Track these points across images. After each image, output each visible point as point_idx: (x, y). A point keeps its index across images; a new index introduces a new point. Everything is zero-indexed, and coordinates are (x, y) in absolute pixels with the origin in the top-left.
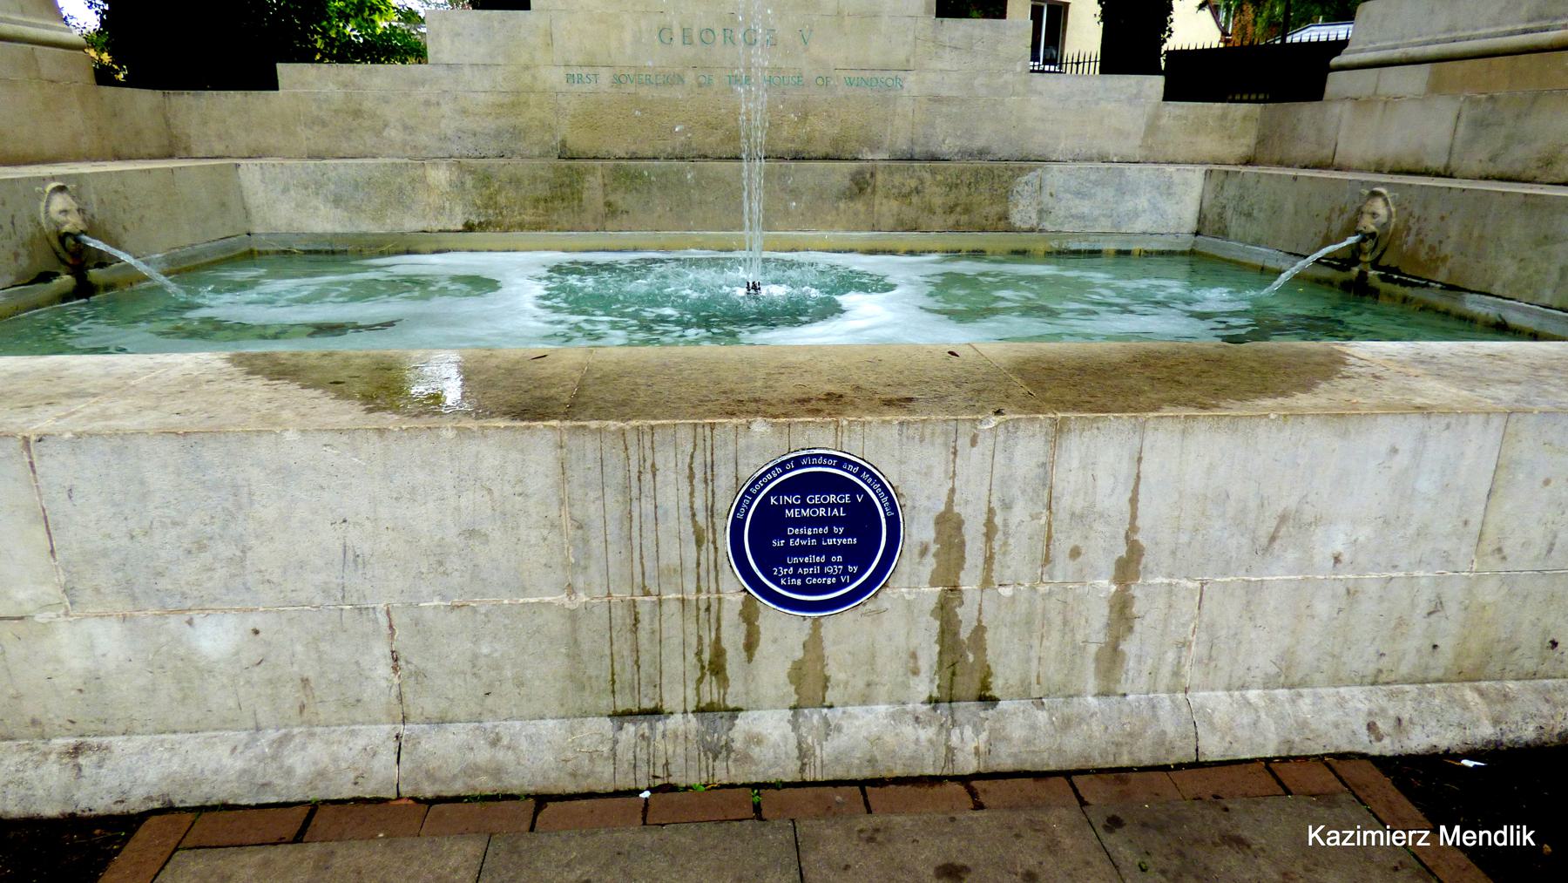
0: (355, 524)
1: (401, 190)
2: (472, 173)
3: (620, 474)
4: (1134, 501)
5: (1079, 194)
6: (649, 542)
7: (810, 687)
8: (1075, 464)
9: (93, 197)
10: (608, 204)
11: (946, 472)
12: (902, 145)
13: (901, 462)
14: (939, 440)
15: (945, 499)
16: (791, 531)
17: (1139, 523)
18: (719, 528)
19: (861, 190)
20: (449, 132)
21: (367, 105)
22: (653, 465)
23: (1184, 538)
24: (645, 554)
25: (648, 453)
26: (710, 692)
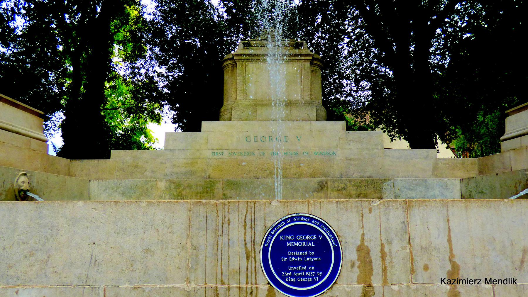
0: (99, 245)
1: (147, 189)
2: (174, 183)
3: (214, 224)
4: (449, 241)
6: (225, 257)
8: (418, 222)
9: (35, 180)
10: (224, 194)
11: (359, 226)
13: (338, 220)
14: (355, 210)
15: (360, 238)
16: (290, 253)
17: (454, 252)
18: (257, 251)
19: (322, 188)
20: (168, 173)
21: (140, 164)
22: (229, 220)
23: (478, 261)
24: (223, 263)
25: (227, 214)
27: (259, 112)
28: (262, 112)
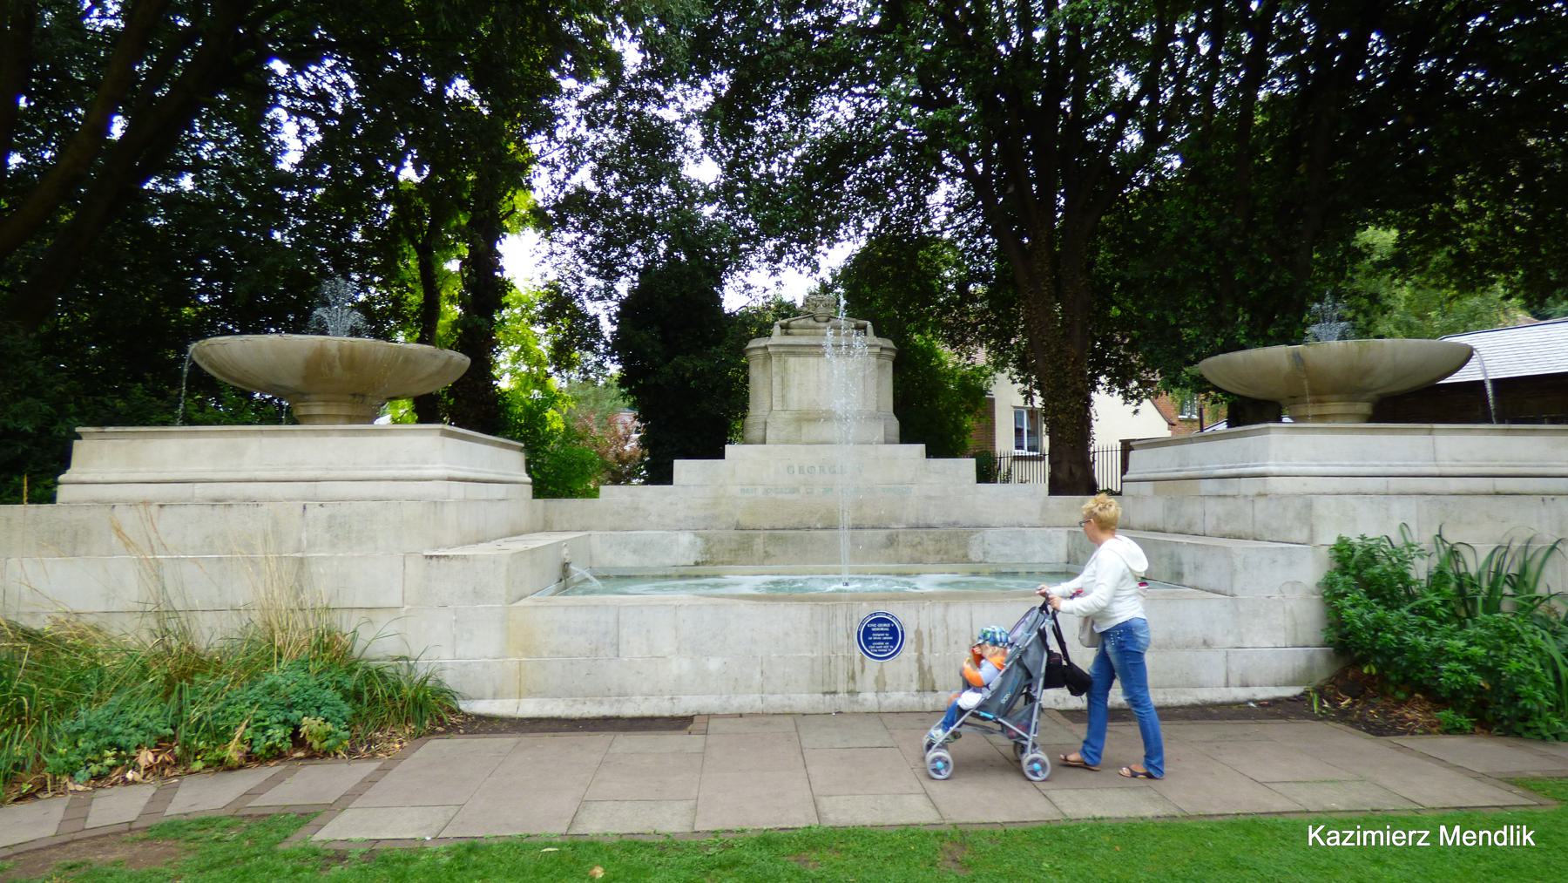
5: (1004, 544)
7: (881, 686)
12: (913, 521)
26: (851, 687)
27: (805, 430)
28: (810, 431)
